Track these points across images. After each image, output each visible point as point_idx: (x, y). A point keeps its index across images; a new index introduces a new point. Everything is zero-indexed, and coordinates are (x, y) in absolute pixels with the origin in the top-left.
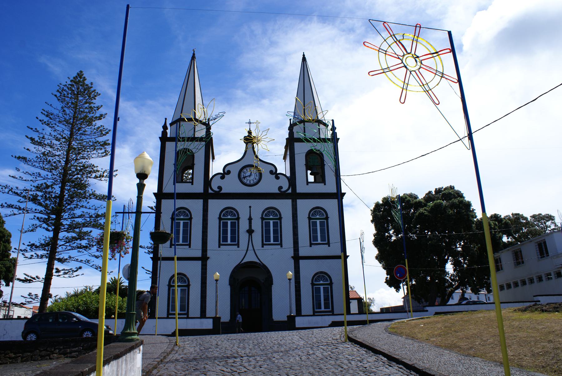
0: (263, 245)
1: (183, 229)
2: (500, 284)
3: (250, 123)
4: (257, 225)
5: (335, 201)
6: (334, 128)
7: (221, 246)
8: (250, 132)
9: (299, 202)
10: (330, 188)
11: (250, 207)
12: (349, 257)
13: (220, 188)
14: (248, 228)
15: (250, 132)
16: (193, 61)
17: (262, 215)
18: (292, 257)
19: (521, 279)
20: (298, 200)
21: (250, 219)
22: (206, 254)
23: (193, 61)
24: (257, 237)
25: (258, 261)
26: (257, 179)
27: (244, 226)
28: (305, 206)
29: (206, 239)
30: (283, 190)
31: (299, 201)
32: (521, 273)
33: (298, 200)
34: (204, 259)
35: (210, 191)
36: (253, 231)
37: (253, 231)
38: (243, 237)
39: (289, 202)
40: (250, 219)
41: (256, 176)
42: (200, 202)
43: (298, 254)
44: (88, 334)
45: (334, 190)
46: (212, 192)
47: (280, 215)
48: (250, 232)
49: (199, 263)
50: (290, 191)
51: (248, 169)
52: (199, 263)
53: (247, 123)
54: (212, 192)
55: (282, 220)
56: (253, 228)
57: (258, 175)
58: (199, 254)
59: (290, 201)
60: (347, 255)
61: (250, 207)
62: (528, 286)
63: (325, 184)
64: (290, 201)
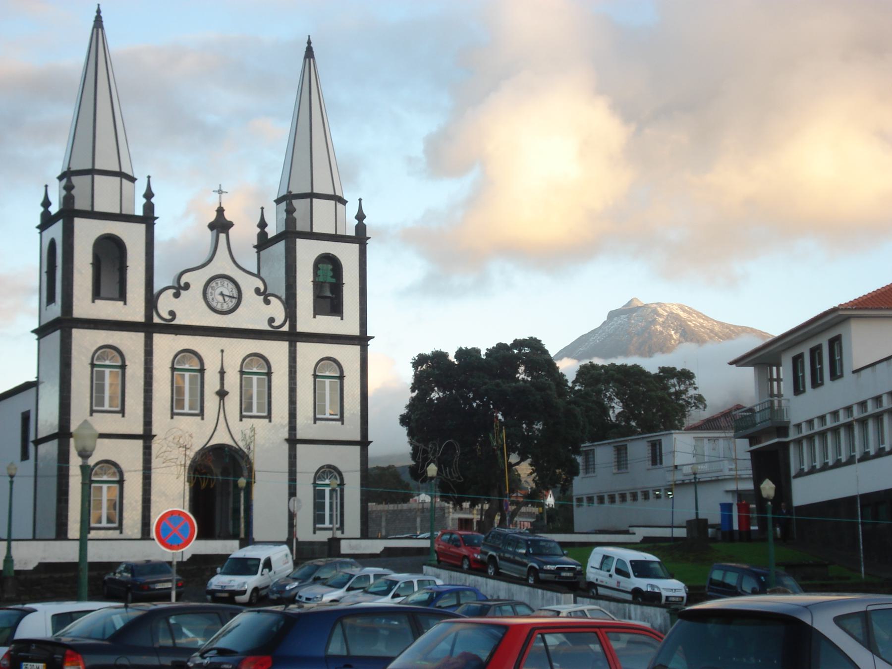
0: (242, 417)
1: (325, 390)
2: (579, 497)
3: (220, 192)
4: (232, 382)
5: (357, 349)
7: (243, 419)
8: (220, 211)
9: (301, 346)
10: (348, 325)
11: (222, 351)
12: (371, 444)
13: (172, 314)
14: (218, 388)
15: (220, 211)
16: (222, 401)
18: (286, 440)
19: (598, 495)
20: (298, 344)
21: (222, 373)
22: (151, 430)
23: (222, 401)
24: (233, 402)
25: (234, 445)
27: (212, 383)
28: (309, 354)
29: (151, 404)
32: (622, 483)
33: (298, 344)
34: (147, 437)
35: (156, 320)
36: (227, 393)
37: (227, 393)
38: (211, 402)
39: (284, 346)
40: (222, 373)
42: (140, 337)
44: (636, 574)
45: (355, 331)
46: (287, 323)
47: (269, 367)
48: (222, 394)
49: (140, 443)
50: (286, 328)
51: (219, 282)
52: (140, 443)
53: (216, 191)
54: (287, 323)
55: (345, 381)
56: (226, 388)
57: (209, 294)
58: (357, 437)
59: (285, 345)
60: (370, 440)
61: (222, 351)
62: (618, 505)
63: (342, 319)
64: (285, 345)
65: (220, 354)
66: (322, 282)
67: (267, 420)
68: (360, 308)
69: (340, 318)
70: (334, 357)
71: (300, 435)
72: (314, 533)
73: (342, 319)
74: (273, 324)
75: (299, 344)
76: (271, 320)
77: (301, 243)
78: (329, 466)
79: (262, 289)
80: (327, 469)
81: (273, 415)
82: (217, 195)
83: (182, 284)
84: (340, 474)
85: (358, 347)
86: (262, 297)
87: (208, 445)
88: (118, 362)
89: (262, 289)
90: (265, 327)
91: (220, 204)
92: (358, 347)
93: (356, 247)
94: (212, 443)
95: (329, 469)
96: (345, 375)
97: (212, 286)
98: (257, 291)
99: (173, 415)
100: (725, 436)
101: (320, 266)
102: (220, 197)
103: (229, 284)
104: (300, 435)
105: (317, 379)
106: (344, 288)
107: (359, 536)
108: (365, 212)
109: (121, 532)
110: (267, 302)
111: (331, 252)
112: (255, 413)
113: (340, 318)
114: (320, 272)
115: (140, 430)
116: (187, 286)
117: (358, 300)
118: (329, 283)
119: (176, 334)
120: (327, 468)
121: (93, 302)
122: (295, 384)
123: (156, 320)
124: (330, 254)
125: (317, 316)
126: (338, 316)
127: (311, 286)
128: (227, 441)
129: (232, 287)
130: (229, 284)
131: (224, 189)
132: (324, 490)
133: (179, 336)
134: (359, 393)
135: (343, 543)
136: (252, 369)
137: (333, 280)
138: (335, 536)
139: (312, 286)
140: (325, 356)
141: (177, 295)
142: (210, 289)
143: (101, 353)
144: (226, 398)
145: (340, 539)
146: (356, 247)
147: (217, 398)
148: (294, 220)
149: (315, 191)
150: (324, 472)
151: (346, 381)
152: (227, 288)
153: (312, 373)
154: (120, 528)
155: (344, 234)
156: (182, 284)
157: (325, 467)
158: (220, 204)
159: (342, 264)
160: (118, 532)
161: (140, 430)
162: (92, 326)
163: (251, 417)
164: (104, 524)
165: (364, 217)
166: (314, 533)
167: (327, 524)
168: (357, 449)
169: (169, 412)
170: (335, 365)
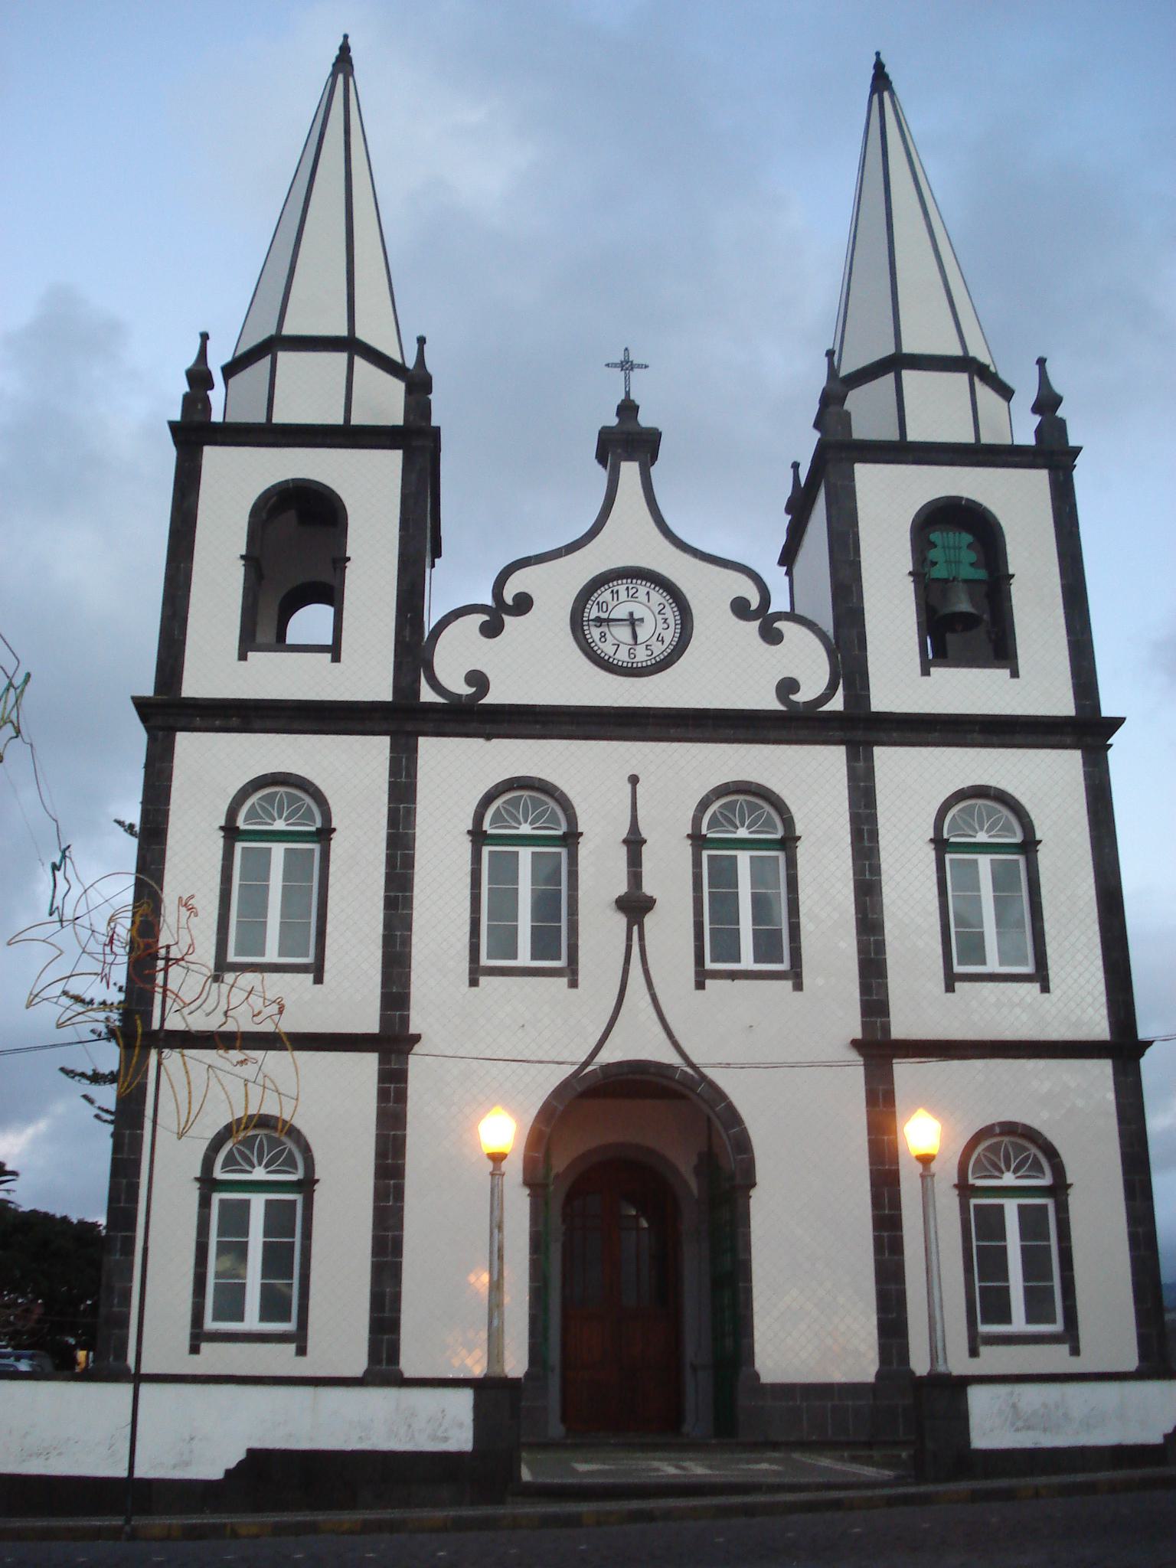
0: (702, 978)
3: (627, 366)
5: (1068, 763)
6: (1047, 403)
11: (634, 780)
12: (1149, 1052)
13: (478, 680)
14: (622, 888)
15: (628, 409)
17: (479, 818)
20: (878, 751)
21: (634, 843)
22: (405, 1021)
23: (635, 928)
26: (667, 643)
30: (801, 697)
31: (883, 755)
35: (427, 695)
36: (648, 904)
37: (648, 904)
40: (634, 843)
41: (661, 625)
42: (377, 749)
43: (886, 1027)
45: (1062, 704)
50: (837, 704)
51: (622, 589)
52: (368, 1064)
53: (615, 365)
56: (648, 888)
57: (671, 622)
61: (634, 780)
63: (1015, 674)
65: (629, 787)
66: (946, 581)
67: (1035, 987)
68: (1069, 642)
69: (1007, 672)
70: (999, 786)
71: (901, 1028)
72: (195, 1349)
73: (1015, 674)
74: (793, 697)
75: (427, 746)
76: (787, 687)
77: (867, 477)
78: (1010, 1128)
79: (755, 603)
80: (1006, 1139)
81: (328, 965)
82: (619, 375)
83: (508, 598)
84: (1051, 1153)
85: (1076, 756)
86: (508, 619)
87: (590, 1068)
88: (1014, 835)
89: (755, 603)
90: (770, 702)
91: (628, 393)
92: (1076, 756)
93: (1039, 479)
94: (606, 1057)
95: (1013, 1139)
96: (1038, 837)
97: (601, 599)
98: (740, 608)
99: (951, 981)
100: (162, 973)
101: (935, 537)
102: (627, 380)
103: (652, 593)
104: (901, 1028)
105: (948, 857)
106: (1013, 589)
107: (1130, 1361)
108: (1058, 386)
109: (1075, 1351)
110: (771, 636)
111: (965, 494)
112: (993, 965)
113: (1007, 672)
114: (933, 554)
115: (369, 1022)
116: (523, 604)
117: (1062, 621)
118: (966, 581)
119: (488, 737)
120: (1001, 1134)
121: (243, 657)
122: (409, 862)
123: (427, 695)
124: (961, 498)
125: (250, 654)
126: (1003, 667)
127: (907, 590)
128: (657, 1051)
129: (663, 601)
130: (652, 593)
131: (635, 358)
132: (1000, 1209)
133: (496, 743)
134: (1092, 893)
135: (978, 1398)
136: (735, 833)
137: (981, 574)
138: (941, 1368)
139: (912, 586)
140: (953, 789)
141: (492, 630)
142: (595, 607)
143: (960, 811)
144: (649, 920)
145: (966, 1381)
146: (1039, 479)
147: (621, 921)
148: (1061, 425)
149: (908, 348)
150: (249, 1142)
151: (1045, 857)
152: (620, 602)
153: (930, 834)
154: (1070, 1336)
155: (1008, 441)
156: (508, 598)
157: (997, 1130)
158: (628, 393)
159: (1003, 524)
160: (1065, 1349)
161: (1099, 1028)
162: (235, 721)
163: (733, 975)
164: (252, 1322)
165: (1057, 401)
166: (195, 1349)
167: (1019, 1323)
168: (1102, 1070)
169: (465, 965)
170: (1005, 812)
